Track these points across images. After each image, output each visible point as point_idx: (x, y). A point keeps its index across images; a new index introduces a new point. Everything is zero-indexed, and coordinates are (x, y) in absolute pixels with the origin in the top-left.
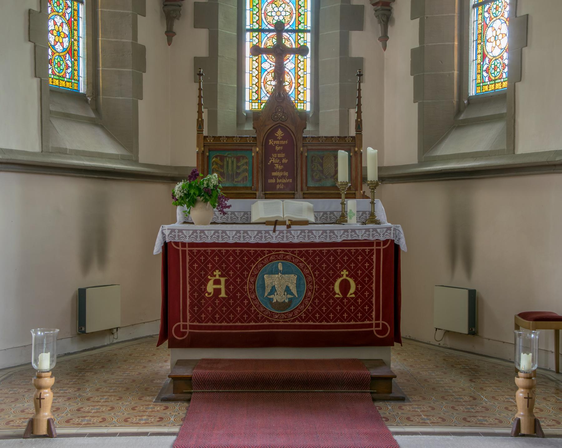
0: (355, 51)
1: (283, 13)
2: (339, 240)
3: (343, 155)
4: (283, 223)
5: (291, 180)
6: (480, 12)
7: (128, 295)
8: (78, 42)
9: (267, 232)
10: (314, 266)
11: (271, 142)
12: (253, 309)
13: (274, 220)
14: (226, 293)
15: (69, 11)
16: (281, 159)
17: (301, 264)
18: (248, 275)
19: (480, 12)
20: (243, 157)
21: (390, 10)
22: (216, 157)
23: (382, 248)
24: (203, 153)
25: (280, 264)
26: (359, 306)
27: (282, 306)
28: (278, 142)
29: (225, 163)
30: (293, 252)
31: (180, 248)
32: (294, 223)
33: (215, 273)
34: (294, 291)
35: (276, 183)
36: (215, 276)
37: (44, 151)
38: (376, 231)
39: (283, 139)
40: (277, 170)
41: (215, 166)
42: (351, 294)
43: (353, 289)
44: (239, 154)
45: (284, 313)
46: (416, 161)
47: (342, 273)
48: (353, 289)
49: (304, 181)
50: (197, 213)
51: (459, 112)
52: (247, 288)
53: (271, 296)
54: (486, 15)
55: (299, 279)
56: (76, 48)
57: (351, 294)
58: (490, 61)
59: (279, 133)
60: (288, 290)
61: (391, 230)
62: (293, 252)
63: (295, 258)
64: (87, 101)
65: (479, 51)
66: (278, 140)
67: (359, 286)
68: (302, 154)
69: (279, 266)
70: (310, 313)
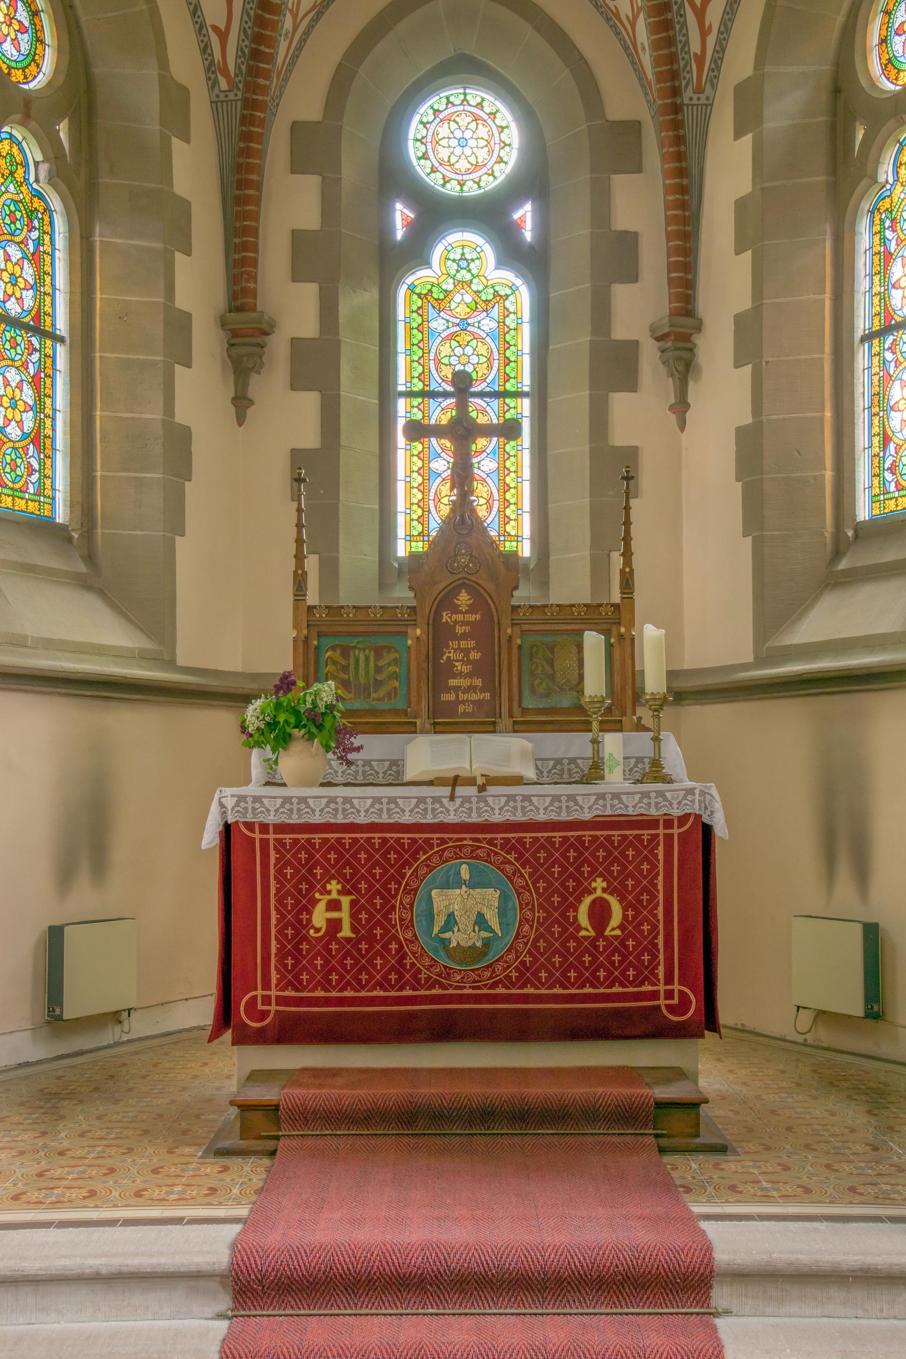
0: (621, 435)
3: (593, 641)
4: (471, 782)
5: (488, 696)
6: (875, 349)
7: (161, 946)
8: (54, 419)
9: (437, 800)
11: (445, 617)
13: (452, 775)
14: (354, 929)
15: (35, 357)
16: (467, 651)
17: (508, 867)
19: (875, 349)
22: (334, 648)
23: (676, 831)
24: (306, 640)
25: (464, 866)
28: (460, 617)
29: (352, 661)
30: (491, 842)
31: (257, 836)
33: (329, 887)
34: (494, 921)
35: (457, 702)
36: (329, 893)
39: (472, 610)
40: (460, 675)
41: (330, 668)
42: (613, 929)
44: (381, 641)
46: (750, 658)
47: (594, 885)
50: (295, 761)
51: (837, 554)
52: (395, 917)
53: (447, 935)
54: (889, 356)
55: (504, 898)
57: (613, 929)
60: (481, 921)
61: (694, 794)
62: (491, 842)
63: (496, 853)
64: (70, 539)
65: (876, 430)
66: (461, 612)
67: (630, 913)
69: (463, 872)
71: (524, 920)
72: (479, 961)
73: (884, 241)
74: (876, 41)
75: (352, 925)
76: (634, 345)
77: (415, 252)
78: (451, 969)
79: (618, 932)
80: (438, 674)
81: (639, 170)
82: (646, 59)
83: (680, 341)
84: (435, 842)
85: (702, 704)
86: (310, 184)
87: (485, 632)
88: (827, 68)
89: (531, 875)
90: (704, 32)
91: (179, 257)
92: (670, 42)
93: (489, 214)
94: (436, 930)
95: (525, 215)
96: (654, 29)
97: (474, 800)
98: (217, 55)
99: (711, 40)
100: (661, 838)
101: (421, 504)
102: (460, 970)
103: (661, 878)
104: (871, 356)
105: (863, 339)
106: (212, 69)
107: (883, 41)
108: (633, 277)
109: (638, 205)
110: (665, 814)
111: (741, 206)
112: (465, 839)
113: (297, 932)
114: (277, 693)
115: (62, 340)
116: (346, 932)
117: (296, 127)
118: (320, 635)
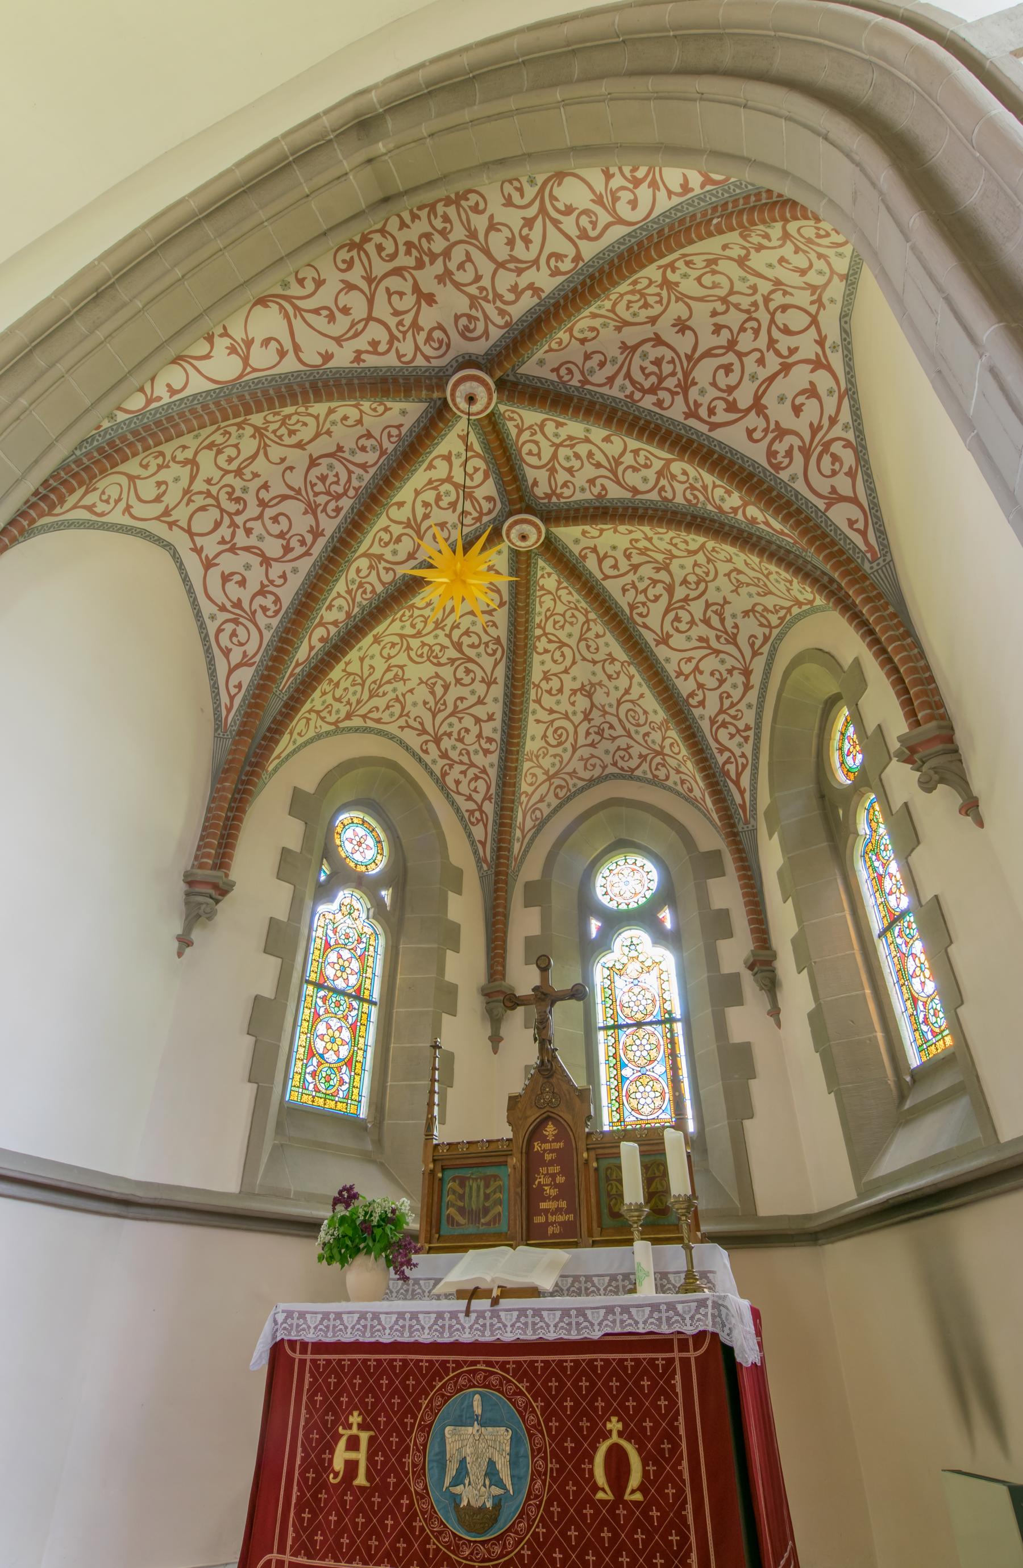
0: (737, 1035)
1: (644, 1002)
2: (596, 1335)
4: (486, 1293)
5: (571, 1217)
6: (890, 940)
8: (365, 1051)
9: (454, 1315)
10: (548, 1404)
11: (537, 1146)
12: (417, 1524)
13: (471, 1287)
14: (369, 1476)
15: (354, 1013)
16: (553, 1176)
17: (520, 1400)
18: (413, 1425)
19: (890, 940)
20: (496, 1177)
21: (773, 971)
22: (454, 1179)
23: (692, 1355)
24: (432, 1172)
25: (477, 1397)
26: (656, 1529)
27: (480, 1518)
28: (547, 1146)
29: (467, 1189)
30: (503, 1366)
31: (297, 1356)
32: (506, 1292)
33: (351, 1419)
34: (505, 1474)
35: (547, 1224)
36: (350, 1426)
37: (246, 1191)
38: (675, 1309)
39: (557, 1139)
40: (548, 1198)
41: (451, 1197)
42: (633, 1492)
43: (635, 1479)
44: (490, 1171)
45: (483, 1543)
46: (854, 1196)
47: (609, 1426)
48: (635, 1479)
49: (595, 1217)
51: (902, 1097)
52: (408, 1460)
53: (458, 1489)
54: (899, 941)
55: (515, 1441)
56: (360, 1058)
57: (633, 1492)
58: (925, 1004)
59: (550, 1130)
60: (491, 1473)
61: (706, 1307)
62: (503, 1366)
63: (509, 1381)
64: (366, 1129)
65: (906, 996)
66: (548, 1141)
67: (651, 1468)
68: (587, 1162)
69: (475, 1403)
70: (541, 1545)
71: (537, 1474)
72: (490, 1527)
73: (875, 869)
74: (838, 765)
75: (368, 1470)
76: (737, 976)
77: (603, 944)
78: (461, 1538)
79: (638, 1497)
80: (531, 1197)
81: (724, 875)
82: (715, 816)
83: (763, 965)
84: (451, 1365)
85: (832, 1242)
86: (535, 912)
87: (565, 1159)
88: (812, 786)
89: (543, 1410)
90: (742, 793)
91: (449, 953)
92: (723, 800)
93: (644, 917)
94: (447, 1483)
95: (666, 916)
96: (712, 794)
97: (488, 1314)
98: (482, 854)
99: (747, 795)
100: (677, 1363)
101: (618, 1099)
102: (470, 1542)
103: (681, 1418)
104: (888, 946)
105: (879, 936)
106: (479, 861)
107: (842, 763)
108: (730, 934)
109: (726, 893)
110: (679, 1333)
111: (780, 874)
112: (478, 1362)
113: (319, 1476)
114: (334, 1204)
115: (375, 1003)
116: (361, 1480)
117: (528, 885)
118: (443, 1169)
